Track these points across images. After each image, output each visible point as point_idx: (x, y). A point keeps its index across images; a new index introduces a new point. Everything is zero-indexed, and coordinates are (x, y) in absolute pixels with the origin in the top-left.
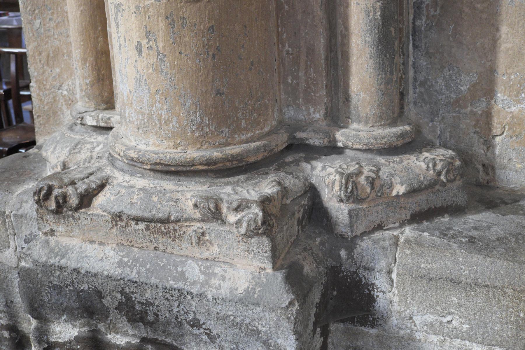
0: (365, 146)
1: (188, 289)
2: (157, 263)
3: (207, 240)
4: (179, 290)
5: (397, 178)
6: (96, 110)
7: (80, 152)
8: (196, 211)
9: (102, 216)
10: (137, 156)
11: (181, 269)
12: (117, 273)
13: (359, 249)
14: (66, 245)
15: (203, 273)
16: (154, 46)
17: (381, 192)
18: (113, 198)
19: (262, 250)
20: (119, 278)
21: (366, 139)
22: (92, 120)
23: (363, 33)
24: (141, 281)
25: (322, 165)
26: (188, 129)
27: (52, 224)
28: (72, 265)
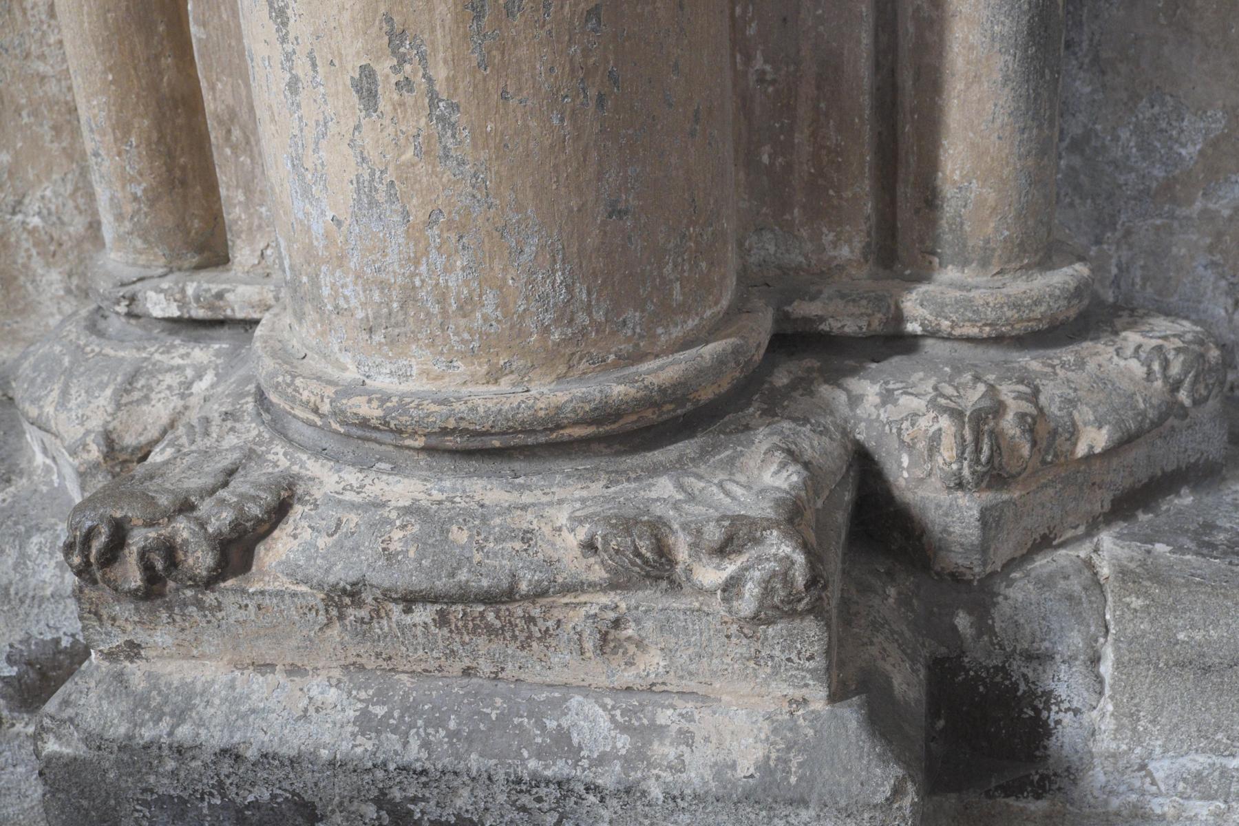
0: (987, 329)
1: (589, 776)
2: (479, 713)
3: (629, 638)
4: (559, 784)
5: (1085, 409)
6: (171, 271)
7: (147, 398)
8: (592, 560)
9: (294, 595)
10: (379, 413)
11: (555, 723)
12: (359, 750)
13: (1003, 608)
14: (184, 684)
15: (625, 729)
16: (419, 80)
17: (1052, 452)
18: (323, 542)
19: (799, 653)
20: (370, 765)
21: (993, 309)
22: (165, 304)
23: (987, 12)
24: (439, 766)
25: (877, 388)
26: (530, 324)
27: (130, 628)
28: (216, 738)
